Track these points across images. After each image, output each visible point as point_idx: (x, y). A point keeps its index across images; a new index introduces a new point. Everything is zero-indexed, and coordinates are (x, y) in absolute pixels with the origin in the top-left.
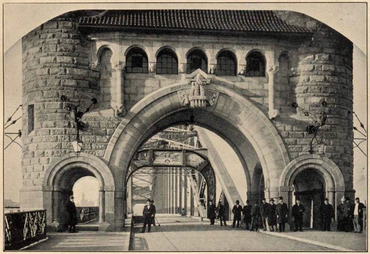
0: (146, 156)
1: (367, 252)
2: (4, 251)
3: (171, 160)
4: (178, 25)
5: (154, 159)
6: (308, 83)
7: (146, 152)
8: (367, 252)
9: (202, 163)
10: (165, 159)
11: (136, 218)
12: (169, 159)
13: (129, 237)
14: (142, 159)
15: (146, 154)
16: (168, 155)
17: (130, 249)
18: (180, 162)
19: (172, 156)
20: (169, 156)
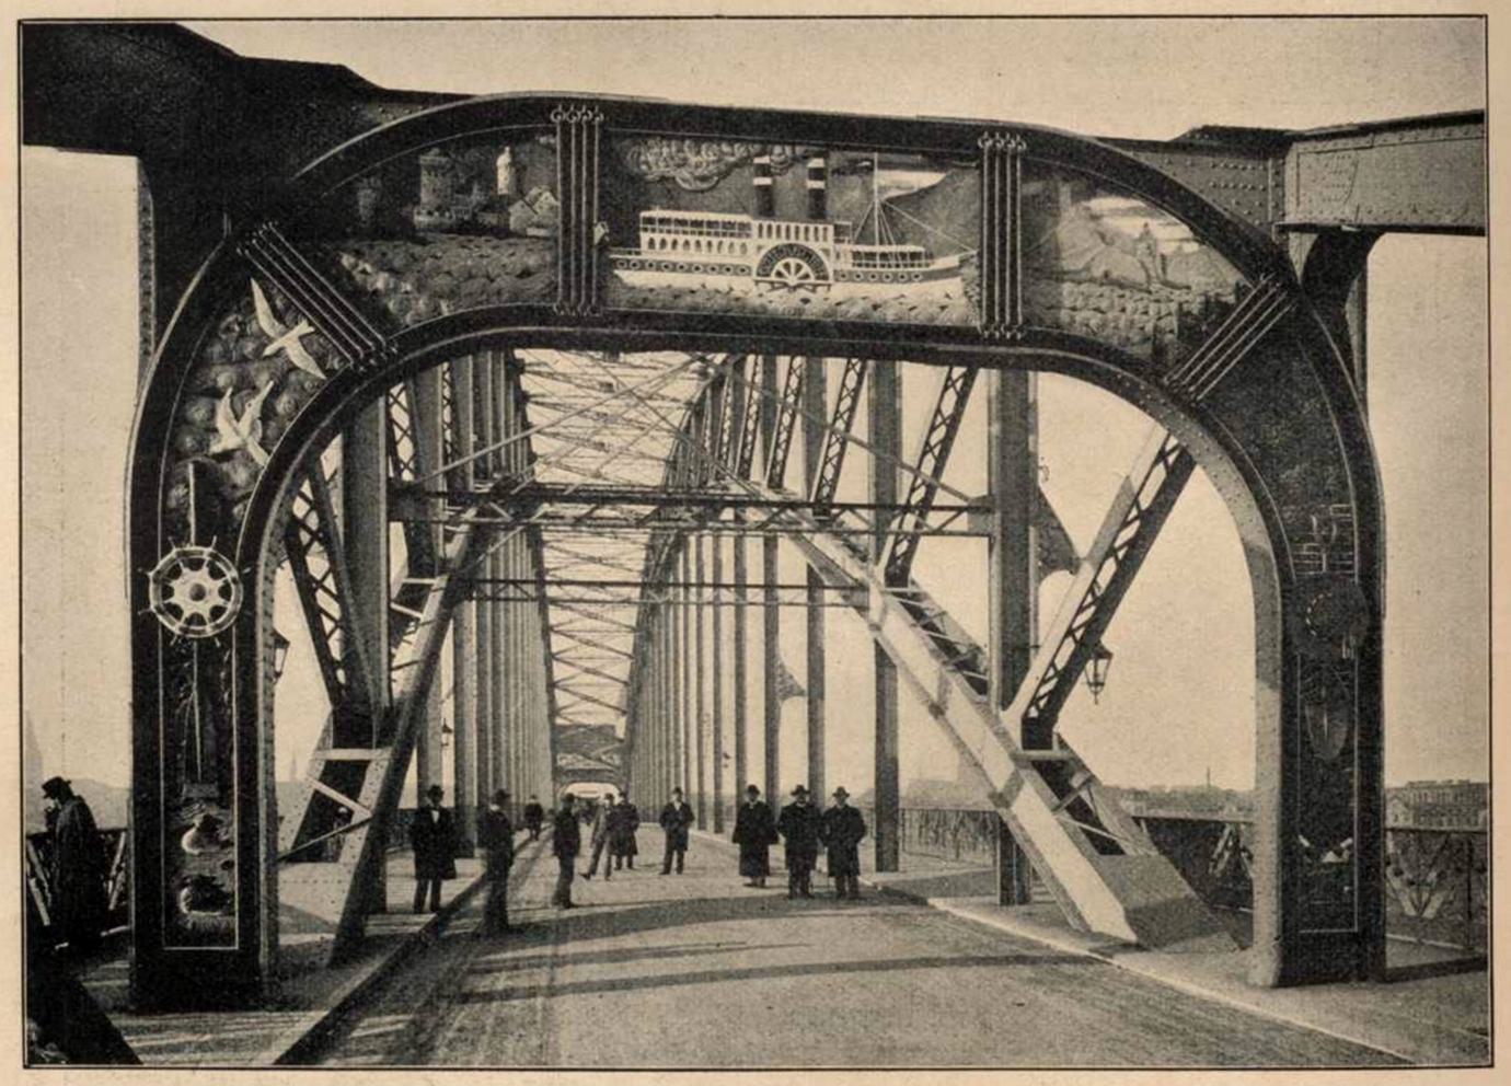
0: (520, 190)
1: (1492, 1066)
2: (25, 1067)
3: (836, 254)
4: (493, 571)
5: (625, 235)
6: (673, 880)
7: (514, 140)
8: (1492, 1066)
9: (1215, 309)
10: (759, 242)
11: (535, 498)
12: (820, 240)
13: (452, 745)
14: (468, 229)
15: (518, 168)
16: (795, 184)
17: (1480, 231)
18: (954, 286)
19: (847, 196)
20: (817, 208)
